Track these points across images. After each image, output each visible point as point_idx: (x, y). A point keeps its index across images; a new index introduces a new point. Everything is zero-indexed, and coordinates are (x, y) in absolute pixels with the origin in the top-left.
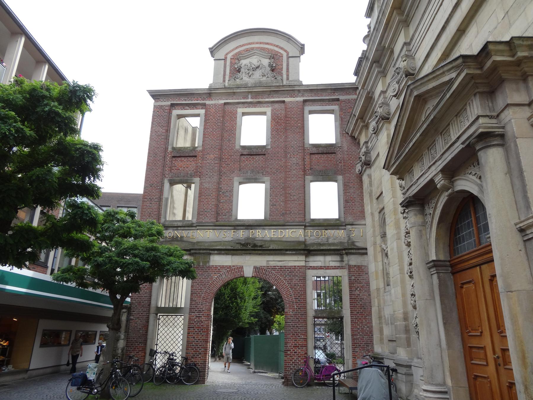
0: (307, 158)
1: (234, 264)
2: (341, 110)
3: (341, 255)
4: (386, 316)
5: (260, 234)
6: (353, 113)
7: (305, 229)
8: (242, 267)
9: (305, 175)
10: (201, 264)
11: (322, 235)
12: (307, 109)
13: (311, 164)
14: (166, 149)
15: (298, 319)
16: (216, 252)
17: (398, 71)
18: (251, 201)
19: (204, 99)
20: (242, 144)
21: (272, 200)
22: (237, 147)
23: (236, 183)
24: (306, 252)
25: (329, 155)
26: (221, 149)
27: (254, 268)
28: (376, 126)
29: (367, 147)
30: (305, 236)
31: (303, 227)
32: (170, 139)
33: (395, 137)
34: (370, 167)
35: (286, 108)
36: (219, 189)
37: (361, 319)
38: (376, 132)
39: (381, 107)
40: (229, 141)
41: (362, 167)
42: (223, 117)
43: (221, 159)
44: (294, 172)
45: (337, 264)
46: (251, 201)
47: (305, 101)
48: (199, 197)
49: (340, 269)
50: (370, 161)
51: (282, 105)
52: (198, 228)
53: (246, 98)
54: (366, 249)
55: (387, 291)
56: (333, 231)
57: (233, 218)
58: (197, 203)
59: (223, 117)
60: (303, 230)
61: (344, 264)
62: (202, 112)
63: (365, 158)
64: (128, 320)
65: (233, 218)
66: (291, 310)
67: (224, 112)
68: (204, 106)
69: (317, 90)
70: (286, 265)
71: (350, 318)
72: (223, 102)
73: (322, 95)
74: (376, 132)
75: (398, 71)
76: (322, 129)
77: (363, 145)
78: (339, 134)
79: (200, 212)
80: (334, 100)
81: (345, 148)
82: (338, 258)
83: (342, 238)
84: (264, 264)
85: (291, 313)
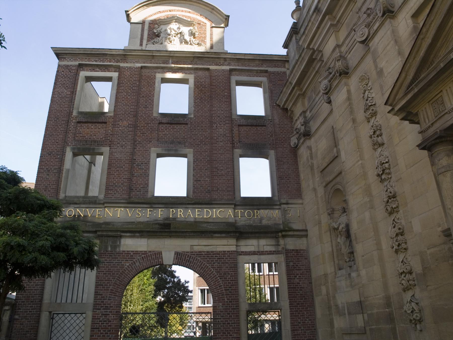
0: (236, 129)
1: (150, 250)
2: (270, 81)
3: (277, 238)
4: (340, 306)
5: (180, 213)
6: (290, 80)
7: (234, 209)
8: (160, 253)
9: (233, 147)
10: (109, 249)
11: (254, 216)
12: (234, 79)
13: (239, 136)
14: (71, 113)
15: (229, 314)
16: (128, 234)
17: (369, 12)
18: (171, 177)
19: (118, 61)
20: (160, 111)
21: (195, 177)
22: (155, 115)
23: (153, 155)
24: (237, 235)
25: (259, 128)
26: (135, 116)
27: (175, 254)
28: (329, 84)
29: (305, 117)
30: (234, 217)
31: (233, 206)
32: (75, 102)
33: (413, 55)
34: (310, 139)
35: (211, 76)
36: (132, 161)
37: (302, 311)
38: (329, 91)
39: (339, 60)
40: (146, 107)
41: (299, 139)
42: (139, 81)
43: (135, 126)
44: (222, 144)
45: (272, 249)
46: (171, 177)
47: (231, 70)
48: (108, 169)
49: (277, 254)
50: (309, 132)
51: (207, 73)
52: (105, 205)
53: (167, 62)
54: (306, 231)
55: (338, 276)
56: (267, 211)
57: (149, 195)
58: (105, 176)
59: (139, 81)
60: (233, 210)
61: (280, 248)
62: (115, 75)
63: (305, 128)
64: (11, 320)
65: (149, 195)
66: (221, 304)
67: (141, 76)
68: (118, 69)
69: (245, 59)
70: (214, 250)
71: (289, 310)
72: (139, 65)
73: (249, 66)
74: (329, 91)
75: (369, 12)
76: (250, 101)
77: (300, 115)
78: (269, 106)
79: (109, 187)
80: (262, 71)
81: (277, 121)
82: (272, 242)
83: (277, 219)
84: (188, 249)
85: (221, 307)
